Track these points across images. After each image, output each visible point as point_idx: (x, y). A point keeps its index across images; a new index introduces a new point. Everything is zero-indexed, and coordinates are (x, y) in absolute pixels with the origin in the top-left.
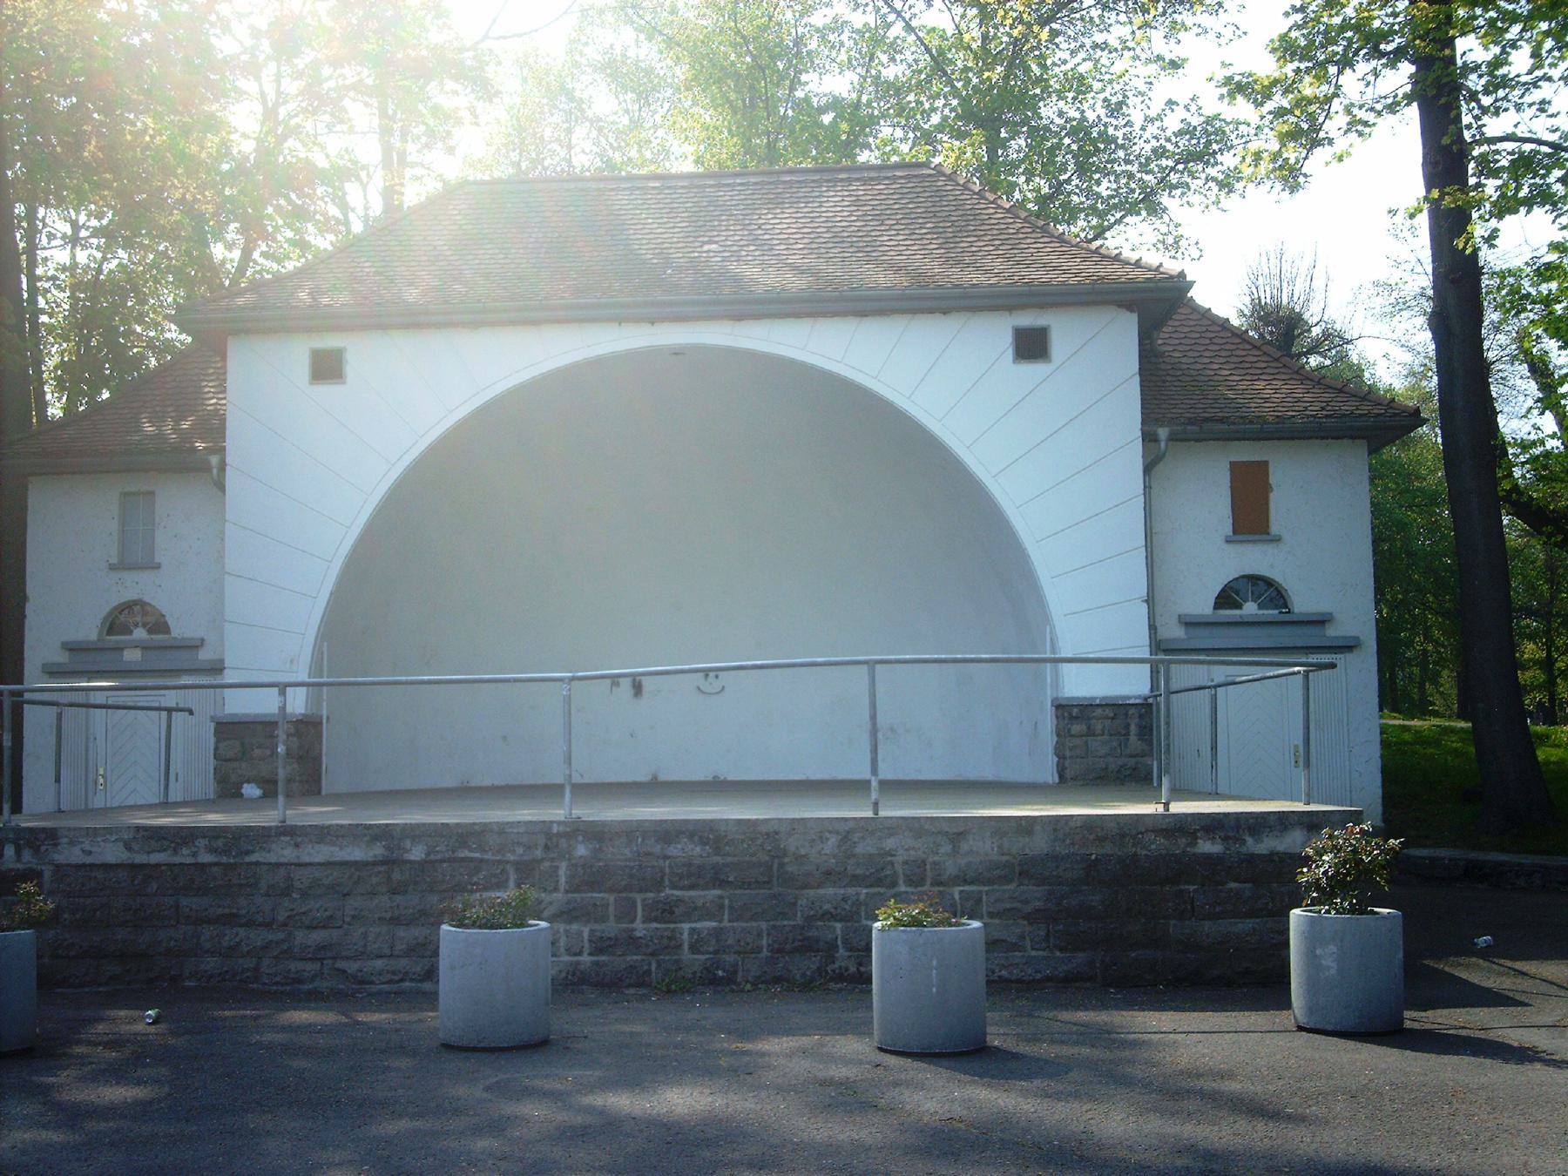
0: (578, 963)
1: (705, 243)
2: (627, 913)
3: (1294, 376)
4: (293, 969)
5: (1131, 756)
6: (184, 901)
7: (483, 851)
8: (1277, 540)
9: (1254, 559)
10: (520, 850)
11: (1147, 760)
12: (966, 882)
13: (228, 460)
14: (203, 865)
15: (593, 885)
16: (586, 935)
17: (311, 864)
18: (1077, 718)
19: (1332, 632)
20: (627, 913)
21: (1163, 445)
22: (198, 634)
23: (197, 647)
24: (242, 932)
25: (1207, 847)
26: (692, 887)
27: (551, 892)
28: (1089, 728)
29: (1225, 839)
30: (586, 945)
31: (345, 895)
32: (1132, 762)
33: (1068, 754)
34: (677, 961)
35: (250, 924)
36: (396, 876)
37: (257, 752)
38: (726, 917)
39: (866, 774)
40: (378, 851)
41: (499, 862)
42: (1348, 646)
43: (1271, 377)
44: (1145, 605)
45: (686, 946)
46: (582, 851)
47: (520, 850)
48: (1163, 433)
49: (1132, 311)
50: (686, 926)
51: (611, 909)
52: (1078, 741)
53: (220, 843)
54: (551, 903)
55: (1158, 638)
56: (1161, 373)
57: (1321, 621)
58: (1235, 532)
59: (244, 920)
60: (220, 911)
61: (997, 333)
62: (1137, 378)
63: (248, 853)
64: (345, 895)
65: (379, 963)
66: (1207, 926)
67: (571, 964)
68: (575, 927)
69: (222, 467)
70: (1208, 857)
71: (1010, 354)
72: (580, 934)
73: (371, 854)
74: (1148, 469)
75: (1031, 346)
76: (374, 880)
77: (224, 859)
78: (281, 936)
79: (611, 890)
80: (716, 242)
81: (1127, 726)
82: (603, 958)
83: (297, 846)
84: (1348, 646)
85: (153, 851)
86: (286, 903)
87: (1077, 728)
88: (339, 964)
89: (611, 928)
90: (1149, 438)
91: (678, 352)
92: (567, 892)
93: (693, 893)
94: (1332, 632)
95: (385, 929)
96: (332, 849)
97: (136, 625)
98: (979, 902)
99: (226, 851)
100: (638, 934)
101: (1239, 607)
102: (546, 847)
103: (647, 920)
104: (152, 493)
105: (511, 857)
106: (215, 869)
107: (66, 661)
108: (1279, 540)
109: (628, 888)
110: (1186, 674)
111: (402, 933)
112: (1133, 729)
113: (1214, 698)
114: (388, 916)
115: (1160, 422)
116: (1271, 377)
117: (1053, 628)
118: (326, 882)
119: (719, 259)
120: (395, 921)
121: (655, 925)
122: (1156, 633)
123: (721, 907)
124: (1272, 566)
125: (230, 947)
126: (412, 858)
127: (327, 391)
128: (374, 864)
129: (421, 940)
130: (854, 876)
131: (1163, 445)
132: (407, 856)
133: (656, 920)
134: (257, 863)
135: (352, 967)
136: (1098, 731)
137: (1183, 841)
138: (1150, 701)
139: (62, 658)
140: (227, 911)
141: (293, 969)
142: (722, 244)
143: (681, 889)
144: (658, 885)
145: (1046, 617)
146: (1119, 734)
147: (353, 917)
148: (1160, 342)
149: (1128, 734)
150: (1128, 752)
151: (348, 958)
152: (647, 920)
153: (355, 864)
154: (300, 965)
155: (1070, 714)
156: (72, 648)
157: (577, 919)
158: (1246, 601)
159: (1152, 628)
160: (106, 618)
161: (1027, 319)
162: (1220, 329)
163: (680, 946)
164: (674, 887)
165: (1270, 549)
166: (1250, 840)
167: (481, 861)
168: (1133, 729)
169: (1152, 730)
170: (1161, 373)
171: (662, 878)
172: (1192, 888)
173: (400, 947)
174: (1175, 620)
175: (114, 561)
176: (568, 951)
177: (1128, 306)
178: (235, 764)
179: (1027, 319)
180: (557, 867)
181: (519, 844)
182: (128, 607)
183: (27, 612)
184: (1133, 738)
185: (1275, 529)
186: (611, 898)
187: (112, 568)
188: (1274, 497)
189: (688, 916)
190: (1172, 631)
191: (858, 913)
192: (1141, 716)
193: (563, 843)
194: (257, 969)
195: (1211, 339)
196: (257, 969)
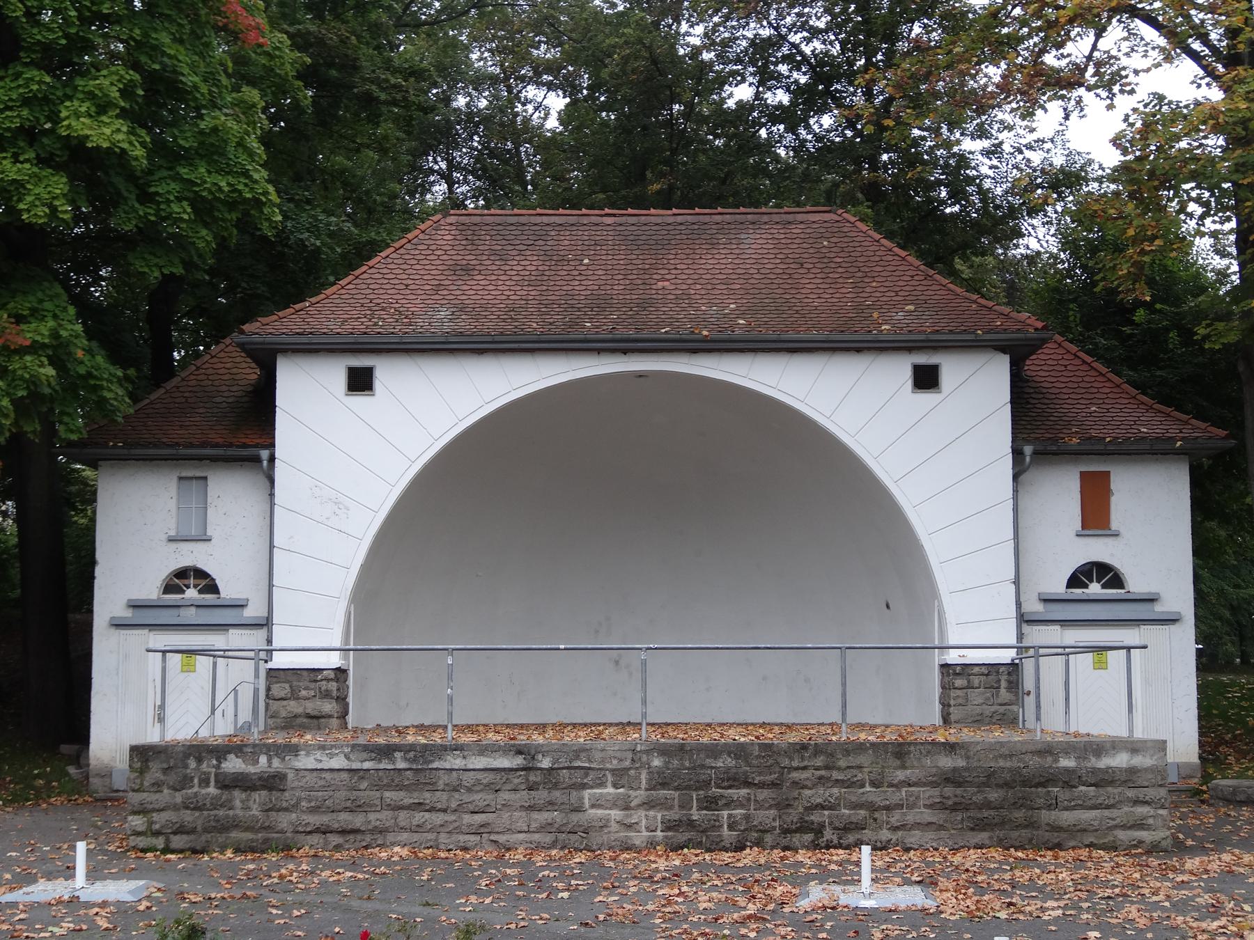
0: (655, 836)
1: (658, 280)
2: (685, 805)
3: (1131, 401)
4: (462, 841)
5: (1001, 705)
6: (387, 794)
7: (590, 761)
8: (1116, 535)
9: (1097, 550)
10: (615, 762)
11: (1015, 708)
12: (910, 785)
13: (277, 455)
14: (400, 770)
15: (664, 785)
16: (659, 818)
17: (474, 770)
18: (959, 674)
19: (1158, 608)
20: (685, 805)
21: (1028, 459)
22: (243, 596)
23: (242, 606)
24: (427, 815)
25: (1067, 763)
26: (730, 787)
27: (636, 790)
28: (969, 682)
29: (1077, 758)
30: (660, 825)
31: (496, 791)
32: (1002, 709)
33: (952, 702)
34: (720, 836)
35: (432, 810)
36: (532, 778)
37: (304, 693)
38: (752, 807)
39: (837, 718)
40: (519, 761)
41: (600, 769)
42: (1172, 620)
43: (1114, 401)
44: (1013, 586)
45: (725, 826)
46: (657, 762)
47: (615, 762)
48: (1028, 450)
49: (1005, 353)
50: (725, 813)
51: (676, 801)
52: (959, 692)
53: (412, 754)
54: (636, 797)
55: (1023, 611)
56: (1026, 396)
57: (1151, 600)
58: (1083, 528)
59: (428, 808)
60: (412, 801)
61: (900, 369)
62: (1009, 405)
63: (432, 761)
64: (496, 791)
65: (522, 836)
66: (1066, 814)
67: (650, 836)
68: (652, 813)
69: (272, 459)
70: (1067, 770)
71: (910, 384)
72: (655, 817)
73: (515, 763)
74: (1016, 477)
75: (926, 379)
76: (516, 781)
77: (414, 766)
78: (453, 818)
79: (676, 789)
80: (668, 280)
81: (999, 681)
82: (670, 834)
83: (464, 757)
84: (1172, 620)
85: (365, 760)
86: (457, 795)
87: (959, 682)
88: (493, 837)
89: (675, 814)
90: (1017, 453)
91: (641, 375)
92: (647, 790)
93: (730, 791)
94: (1158, 608)
95: (524, 814)
96: (489, 759)
97: (188, 587)
98: (918, 798)
99: (415, 760)
100: (694, 818)
101: (1086, 586)
102: (633, 760)
103: (700, 809)
104: (206, 478)
105: (609, 766)
106: (408, 772)
107: (130, 615)
108: (1117, 535)
109: (688, 788)
110: (1040, 635)
111: (535, 815)
112: (1003, 684)
113: (1067, 662)
114: (527, 805)
115: (1028, 442)
116: (1114, 401)
117: (940, 603)
118: (485, 781)
119: (673, 297)
120: (531, 808)
121: (705, 812)
122: (1020, 608)
123: (749, 800)
124: (1112, 555)
125: (418, 826)
126: (543, 766)
127: (359, 401)
128: (517, 770)
129: (550, 821)
130: (837, 780)
131: (1028, 459)
132: (539, 765)
133: (706, 808)
134: (437, 769)
135: (502, 839)
136: (976, 685)
137: (1049, 759)
138: (1017, 661)
139: (128, 613)
140: (416, 801)
141: (462, 841)
142: (673, 281)
143: (723, 788)
144: (706, 784)
145: (933, 593)
146: (992, 687)
147: (503, 805)
148: (1026, 368)
149: (999, 688)
150: (999, 701)
151: (498, 833)
152: (700, 809)
153: (504, 770)
154: (467, 837)
155: (955, 671)
156: (135, 606)
157: (652, 807)
158: (1091, 581)
159: (1019, 604)
160: (164, 580)
161: (923, 359)
162: (1073, 357)
163: (721, 826)
164: (718, 787)
165: (1109, 541)
166: (1093, 759)
167: (590, 768)
168: (1003, 684)
169: (1018, 685)
170: (1026, 396)
171: (711, 780)
172: (1056, 789)
173: (534, 825)
174: (1035, 596)
175: (173, 533)
176: (648, 829)
177: (1001, 349)
178: (285, 703)
179: (923, 359)
180: (640, 773)
181: (615, 758)
182: (182, 574)
183: (97, 573)
184: (1003, 691)
185: (1115, 524)
186: (676, 794)
187: (171, 540)
188: (1114, 500)
189: (728, 805)
190: (1033, 607)
191: (839, 805)
192: (1009, 674)
193: (644, 758)
194: (436, 840)
195: (1066, 366)
196: (436, 840)
